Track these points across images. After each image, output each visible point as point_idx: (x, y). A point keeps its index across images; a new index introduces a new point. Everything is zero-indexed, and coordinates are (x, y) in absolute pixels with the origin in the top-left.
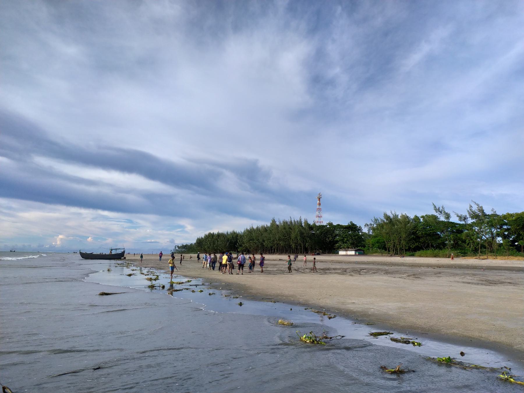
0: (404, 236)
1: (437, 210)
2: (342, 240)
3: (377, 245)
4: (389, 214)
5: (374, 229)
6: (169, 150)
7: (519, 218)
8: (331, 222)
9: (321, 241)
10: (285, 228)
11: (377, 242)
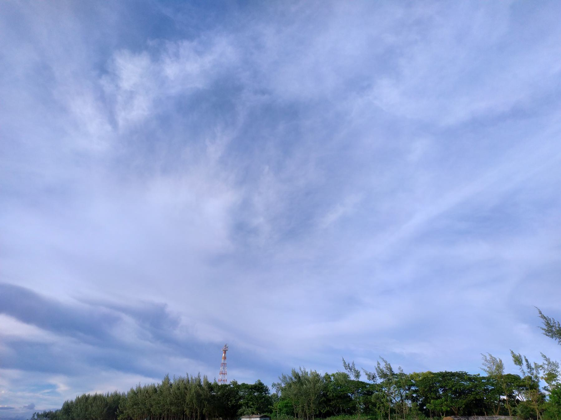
0: (313, 398)
1: (347, 366)
2: (247, 404)
3: (285, 409)
4: (298, 371)
5: (283, 390)
6: (58, 288)
7: (425, 378)
8: (236, 380)
10: (179, 389)
11: (286, 406)
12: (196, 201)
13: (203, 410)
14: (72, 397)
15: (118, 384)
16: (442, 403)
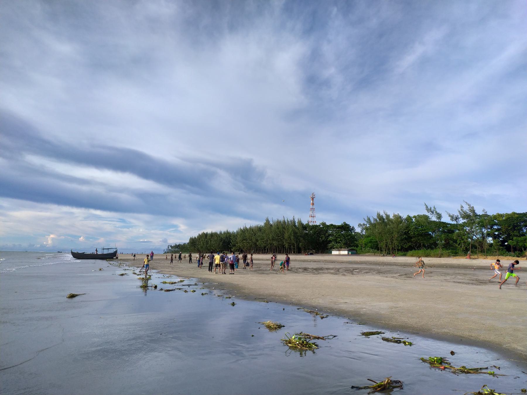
1: (429, 210)
3: (369, 244)
6: (163, 149)
7: (509, 218)
9: (316, 240)
10: (278, 228)
11: (370, 242)
14: (195, 234)
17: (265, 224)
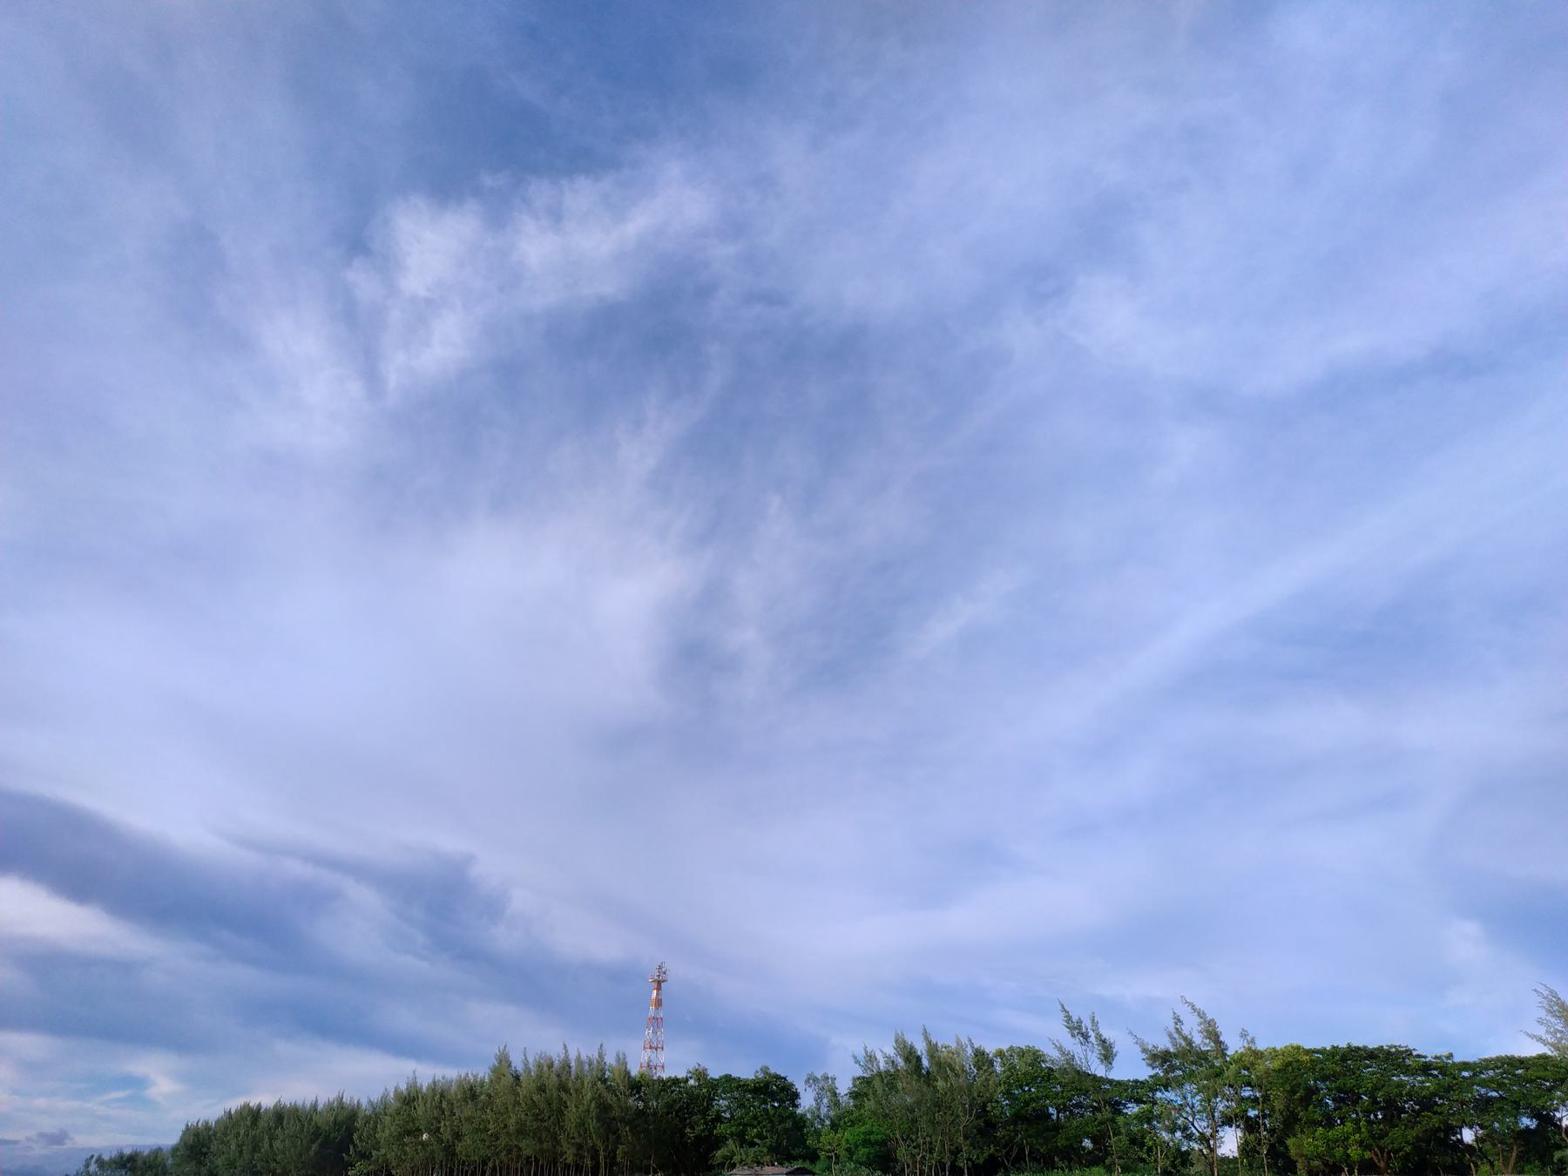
0: (964, 1120)
1: (1076, 1029)
3: (863, 1151)
6: (181, 809)
7: (1290, 1064)
10: (542, 1089)
11: (866, 1143)
12: (580, 584)
13: (614, 1151)
14: (210, 1109)
15: (359, 1078)
16: (1347, 1139)
17: (495, 1070)
